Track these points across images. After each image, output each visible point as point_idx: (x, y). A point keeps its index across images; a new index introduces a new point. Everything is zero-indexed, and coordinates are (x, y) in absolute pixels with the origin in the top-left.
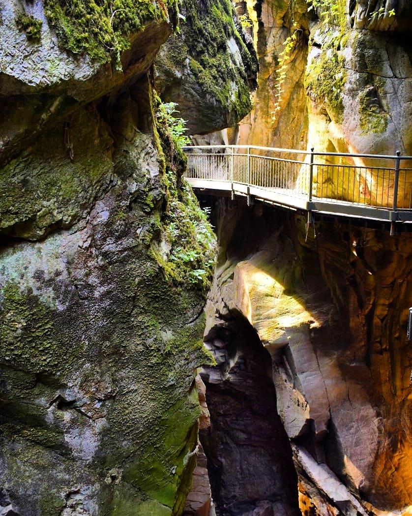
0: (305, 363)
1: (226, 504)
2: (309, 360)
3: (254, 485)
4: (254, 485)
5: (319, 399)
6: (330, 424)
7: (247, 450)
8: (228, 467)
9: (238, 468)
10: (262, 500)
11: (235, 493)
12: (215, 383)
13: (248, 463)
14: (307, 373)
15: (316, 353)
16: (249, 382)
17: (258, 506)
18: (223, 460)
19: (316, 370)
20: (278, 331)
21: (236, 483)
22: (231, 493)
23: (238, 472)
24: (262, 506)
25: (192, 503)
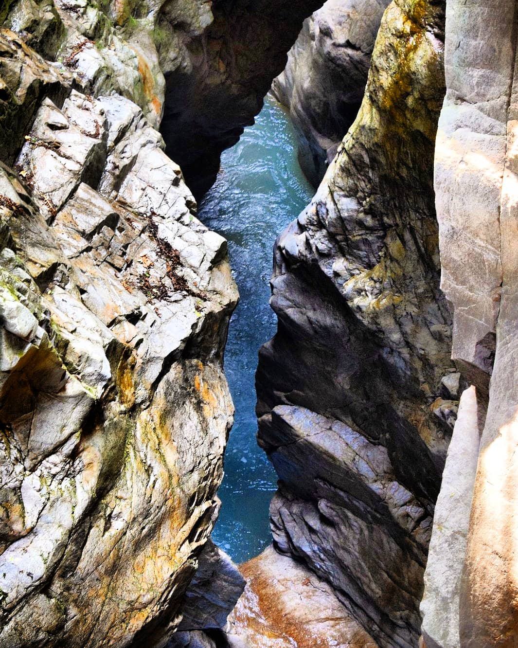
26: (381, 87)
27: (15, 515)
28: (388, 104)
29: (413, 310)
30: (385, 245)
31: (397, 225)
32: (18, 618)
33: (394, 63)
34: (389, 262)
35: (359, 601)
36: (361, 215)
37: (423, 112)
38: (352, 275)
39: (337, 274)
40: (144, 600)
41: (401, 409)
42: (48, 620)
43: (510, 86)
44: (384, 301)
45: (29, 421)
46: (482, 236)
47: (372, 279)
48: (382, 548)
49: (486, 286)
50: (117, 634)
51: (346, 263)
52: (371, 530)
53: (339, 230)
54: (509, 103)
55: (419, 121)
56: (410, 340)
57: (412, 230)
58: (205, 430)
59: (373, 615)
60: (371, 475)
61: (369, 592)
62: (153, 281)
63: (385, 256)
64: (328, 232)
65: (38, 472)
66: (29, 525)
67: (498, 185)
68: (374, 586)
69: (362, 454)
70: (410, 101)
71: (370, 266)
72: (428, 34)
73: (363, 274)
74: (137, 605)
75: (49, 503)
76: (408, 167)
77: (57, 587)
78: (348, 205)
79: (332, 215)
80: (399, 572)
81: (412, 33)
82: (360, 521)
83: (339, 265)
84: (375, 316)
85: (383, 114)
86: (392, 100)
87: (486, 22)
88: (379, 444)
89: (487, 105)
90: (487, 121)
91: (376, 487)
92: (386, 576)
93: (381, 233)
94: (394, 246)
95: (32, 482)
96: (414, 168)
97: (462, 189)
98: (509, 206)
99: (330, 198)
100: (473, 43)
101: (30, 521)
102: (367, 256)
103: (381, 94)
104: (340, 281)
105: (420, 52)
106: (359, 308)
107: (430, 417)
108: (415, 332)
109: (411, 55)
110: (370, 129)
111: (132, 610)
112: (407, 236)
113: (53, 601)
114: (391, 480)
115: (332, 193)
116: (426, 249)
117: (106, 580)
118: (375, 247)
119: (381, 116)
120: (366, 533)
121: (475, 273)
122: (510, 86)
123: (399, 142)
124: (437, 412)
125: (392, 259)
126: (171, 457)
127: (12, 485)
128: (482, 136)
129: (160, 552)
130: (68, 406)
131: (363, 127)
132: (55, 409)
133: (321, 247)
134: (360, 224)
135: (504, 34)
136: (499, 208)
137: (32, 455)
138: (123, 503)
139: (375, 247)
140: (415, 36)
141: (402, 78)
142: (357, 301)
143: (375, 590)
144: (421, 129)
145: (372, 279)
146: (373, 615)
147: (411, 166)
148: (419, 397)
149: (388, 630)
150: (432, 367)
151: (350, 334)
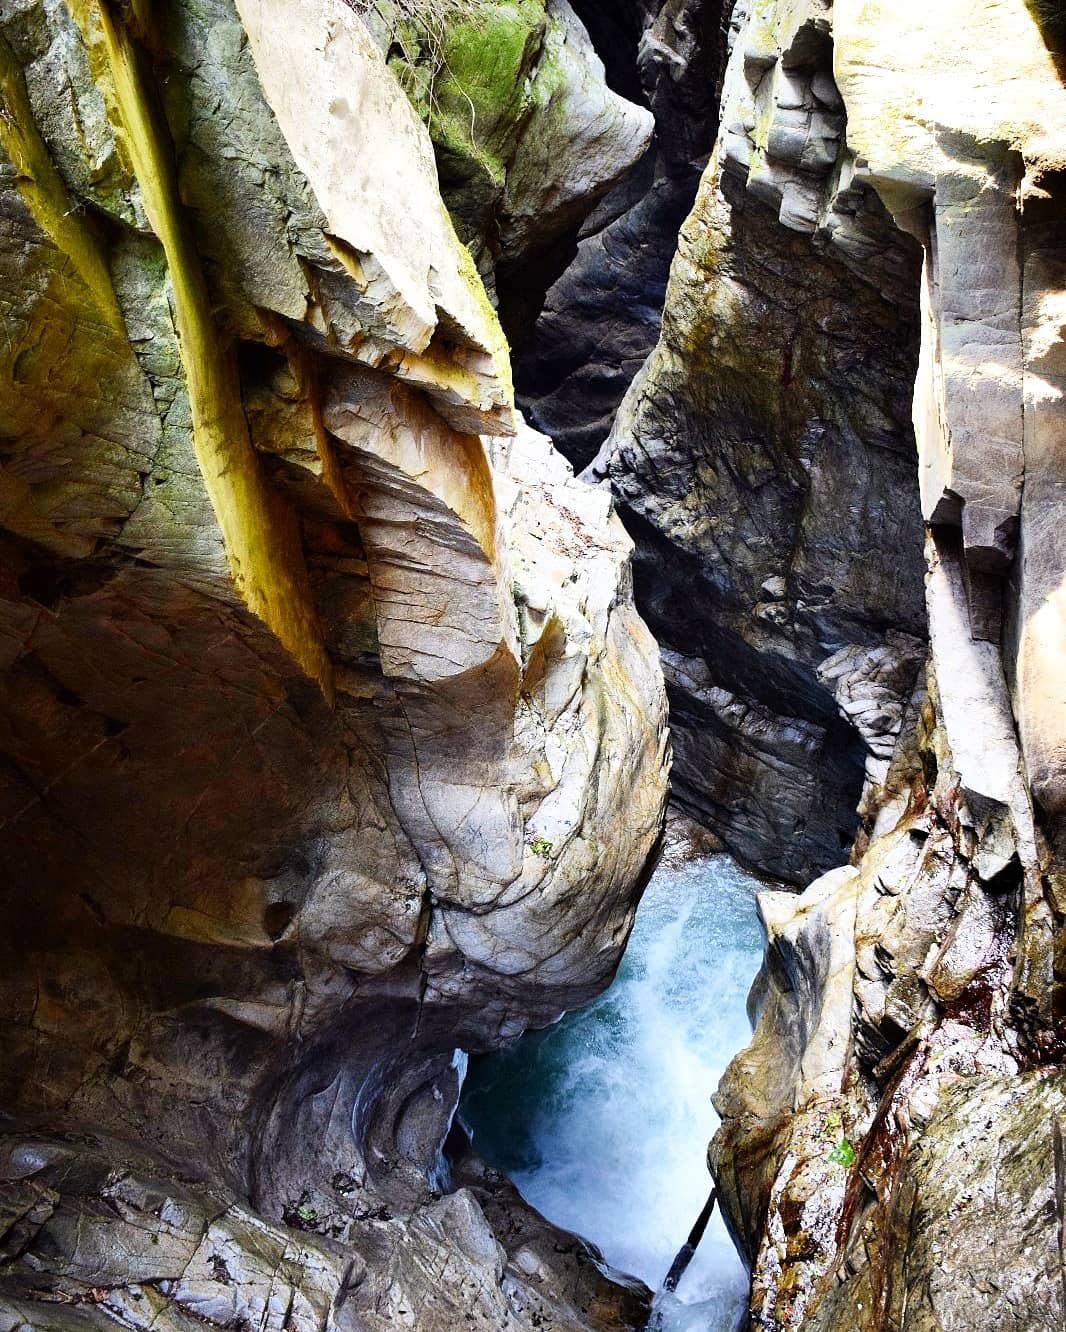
0: (977, 287)
1: (804, 600)
2: (993, 281)
3: (891, 578)
4: (891, 578)
5: (994, 433)
6: (1011, 531)
7: (890, 465)
8: (824, 498)
9: (854, 510)
10: (905, 632)
11: (833, 583)
12: (795, 227)
13: (888, 508)
14: (977, 325)
15: (1021, 259)
16: (893, 262)
17: (886, 645)
18: (816, 471)
19: (1007, 329)
20: (910, 132)
21: (842, 553)
22: (823, 575)
23: (854, 522)
24: (899, 649)
25: (418, 659)
26: (681, 333)
27: (544, 774)
28: (691, 348)
29: (730, 529)
30: (697, 476)
31: (707, 455)
32: (564, 863)
33: (692, 310)
34: (701, 491)
35: (691, 800)
36: (670, 453)
37: (731, 349)
38: (665, 509)
39: (649, 511)
40: (647, 825)
41: (721, 620)
42: (586, 860)
43: (1021, 299)
44: (703, 526)
45: (542, 686)
46: (1001, 434)
47: (687, 508)
48: (709, 748)
49: (1006, 477)
50: (634, 859)
51: (657, 500)
52: (695, 735)
53: (649, 470)
54: (1021, 314)
55: (727, 358)
56: (728, 556)
57: (724, 458)
58: (647, 667)
59: (707, 808)
60: (694, 685)
61: (702, 789)
62: (569, 544)
63: (697, 485)
64: (637, 475)
65: (554, 731)
66: (556, 780)
67: (1019, 386)
68: (706, 784)
69: (681, 668)
70: (715, 341)
71: (682, 497)
72: (725, 279)
73: (676, 507)
74: (642, 831)
75: (569, 756)
76: (717, 401)
77: (587, 830)
78: (656, 447)
79: (640, 458)
80: (730, 766)
81: (707, 280)
82: (683, 729)
83: (651, 502)
84: (695, 540)
85: (687, 358)
86: (695, 342)
87: (987, 247)
88: (695, 657)
89: (995, 320)
90: (998, 333)
91: (699, 695)
92: (716, 772)
93: (690, 466)
94: (707, 475)
95: (552, 740)
96: (724, 401)
97: (979, 397)
98: (1034, 402)
99: (635, 443)
100: (973, 267)
101: (556, 775)
102: (678, 489)
103: (682, 340)
104: (653, 516)
105: (720, 295)
106: (678, 537)
107: (752, 620)
108: (733, 548)
109: (711, 300)
110: (674, 374)
111: (640, 836)
112: (719, 463)
113: (587, 841)
114: (711, 686)
115: (637, 439)
116: (740, 472)
117: (618, 815)
118: (685, 479)
119: (684, 360)
120: (691, 738)
121: (992, 467)
122: (1021, 299)
123: (707, 380)
124: (763, 615)
125: (705, 487)
126: (635, 696)
127: (538, 747)
128: (993, 347)
129: (648, 780)
130: (571, 664)
131: (666, 373)
132: (560, 671)
133: (630, 489)
134: (670, 461)
135: (1007, 254)
136: (1022, 406)
137: (549, 716)
138: (614, 743)
139: (685, 479)
140: (711, 283)
141: (704, 322)
142: (675, 531)
143: (708, 786)
144: (731, 364)
145: (687, 508)
146: (707, 808)
147: (721, 398)
148: (738, 606)
149: (724, 820)
150: (750, 577)
151: (666, 562)
